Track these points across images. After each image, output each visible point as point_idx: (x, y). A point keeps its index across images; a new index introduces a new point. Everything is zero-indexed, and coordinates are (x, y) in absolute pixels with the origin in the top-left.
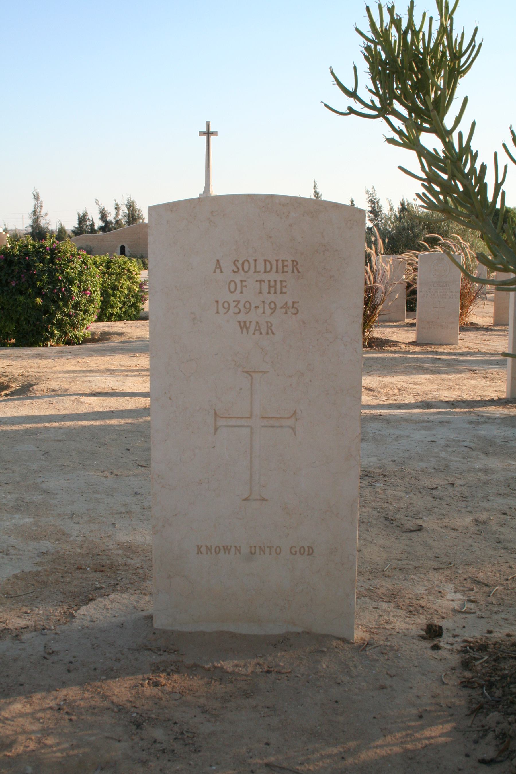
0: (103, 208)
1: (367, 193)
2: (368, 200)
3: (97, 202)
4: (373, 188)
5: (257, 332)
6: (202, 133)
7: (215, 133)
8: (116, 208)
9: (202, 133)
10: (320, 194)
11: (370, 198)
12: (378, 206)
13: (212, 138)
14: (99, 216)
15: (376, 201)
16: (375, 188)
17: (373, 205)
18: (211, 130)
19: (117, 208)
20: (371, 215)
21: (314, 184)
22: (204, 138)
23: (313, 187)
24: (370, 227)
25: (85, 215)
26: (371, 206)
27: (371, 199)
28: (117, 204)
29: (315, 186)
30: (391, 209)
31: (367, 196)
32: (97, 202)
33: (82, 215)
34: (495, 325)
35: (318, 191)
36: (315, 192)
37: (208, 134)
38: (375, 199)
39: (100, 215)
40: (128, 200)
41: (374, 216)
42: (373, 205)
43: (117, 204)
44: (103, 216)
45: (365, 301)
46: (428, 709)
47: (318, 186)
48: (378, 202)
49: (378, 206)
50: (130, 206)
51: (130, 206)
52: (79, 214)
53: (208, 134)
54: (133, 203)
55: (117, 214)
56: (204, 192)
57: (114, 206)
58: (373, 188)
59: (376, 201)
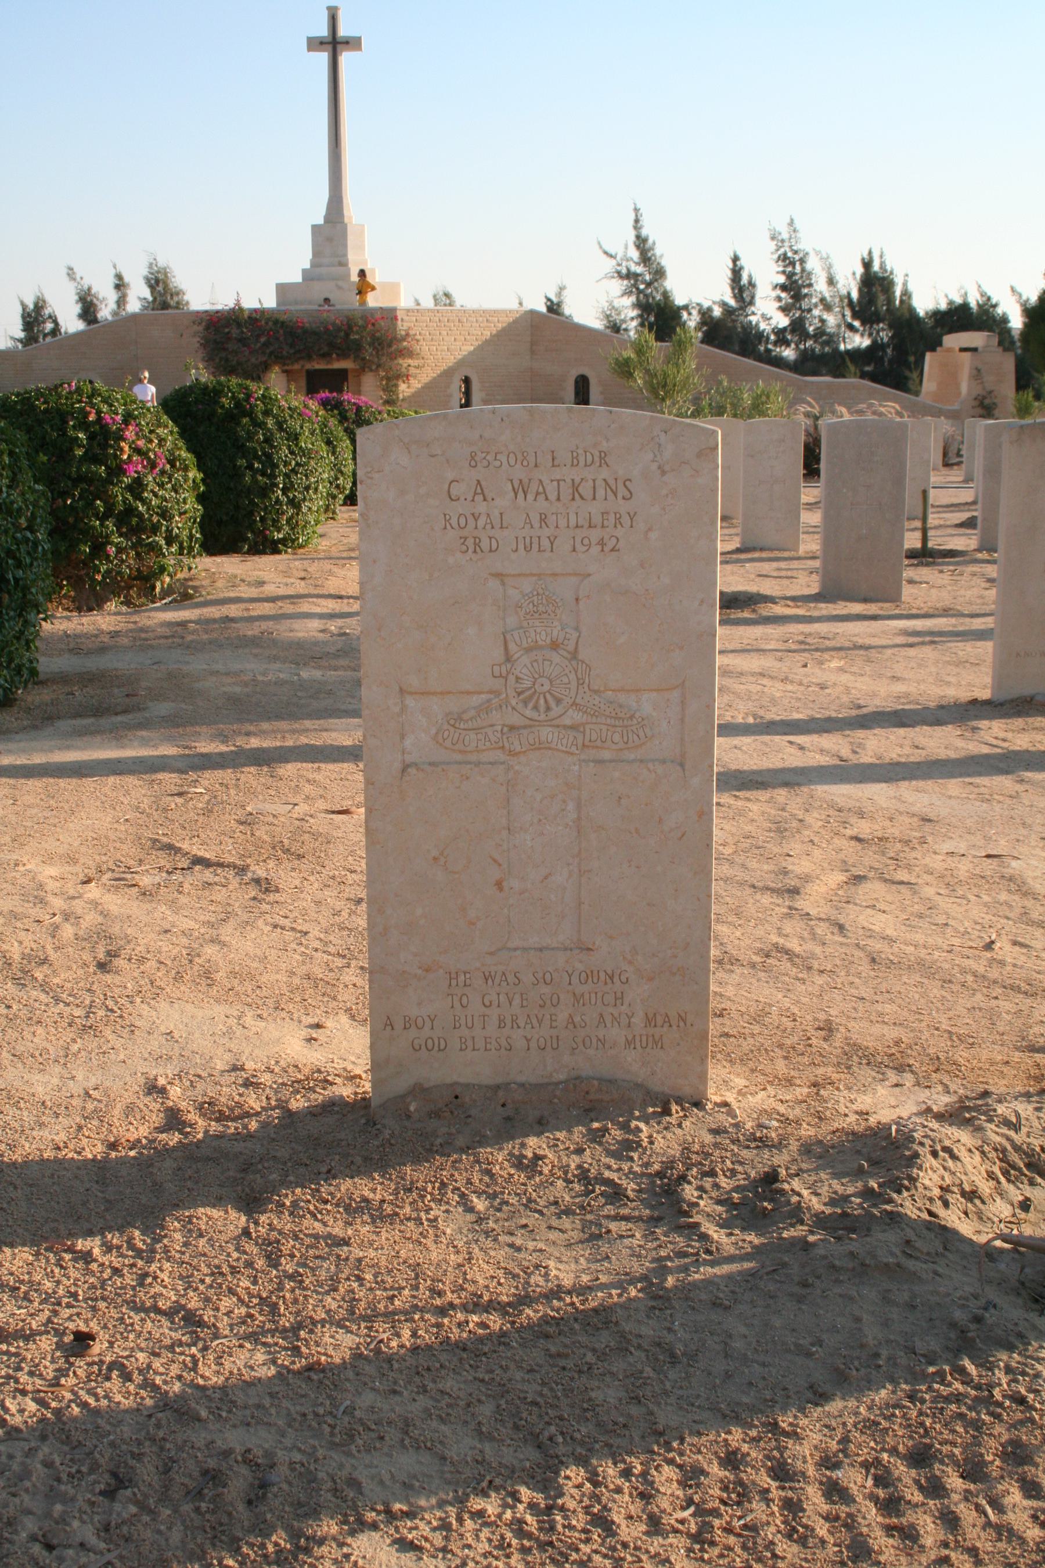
0: (86, 287)
1: (773, 238)
2: (776, 256)
3: (71, 274)
4: (791, 223)
5: (542, 497)
6: (315, 44)
7: (353, 43)
8: (118, 287)
9: (315, 44)
10: (650, 241)
11: (781, 251)
12: (803, 270)
13: (346, 58)
14: (77, 309)
15: (797, 257)
16: (797, 224)
17: (790, 269)
18: (343, 32)
19: (120, 285)
20: (783, 295)
21: (633, 217)
22: (323, 58)
23: (632, 223)
24: (780, 326)
25: (40, 306)
26: (784, 272)
27: (785, 254)
28: (119, 277)
29: (637, 221)
30: (831, 282)
31: (772, 245)
32: (71, 274)
33: (31, 306)
34: (979, 550)
35: (644, 232)
36: (638, 237)
37: (334, 45)
38: (796, 252)
39: (80, 305)
40: (151, 266)
41: (792, 297)
42: (790, 269)
43: (119, 277)
44: (88, 309)
45: (23, 317)
46: (837, 1263)
47: (645, 221)
48: (802, 261)
49: (803, 270)
50: (157, 281)
51: (157, 281)
52: (23, 304)
53: (334, 45)
54: (166, 274)
55: (121, 302)
56: (328, 219)
57: (111, 281)
58: (791, 223)
59: (797, 257)
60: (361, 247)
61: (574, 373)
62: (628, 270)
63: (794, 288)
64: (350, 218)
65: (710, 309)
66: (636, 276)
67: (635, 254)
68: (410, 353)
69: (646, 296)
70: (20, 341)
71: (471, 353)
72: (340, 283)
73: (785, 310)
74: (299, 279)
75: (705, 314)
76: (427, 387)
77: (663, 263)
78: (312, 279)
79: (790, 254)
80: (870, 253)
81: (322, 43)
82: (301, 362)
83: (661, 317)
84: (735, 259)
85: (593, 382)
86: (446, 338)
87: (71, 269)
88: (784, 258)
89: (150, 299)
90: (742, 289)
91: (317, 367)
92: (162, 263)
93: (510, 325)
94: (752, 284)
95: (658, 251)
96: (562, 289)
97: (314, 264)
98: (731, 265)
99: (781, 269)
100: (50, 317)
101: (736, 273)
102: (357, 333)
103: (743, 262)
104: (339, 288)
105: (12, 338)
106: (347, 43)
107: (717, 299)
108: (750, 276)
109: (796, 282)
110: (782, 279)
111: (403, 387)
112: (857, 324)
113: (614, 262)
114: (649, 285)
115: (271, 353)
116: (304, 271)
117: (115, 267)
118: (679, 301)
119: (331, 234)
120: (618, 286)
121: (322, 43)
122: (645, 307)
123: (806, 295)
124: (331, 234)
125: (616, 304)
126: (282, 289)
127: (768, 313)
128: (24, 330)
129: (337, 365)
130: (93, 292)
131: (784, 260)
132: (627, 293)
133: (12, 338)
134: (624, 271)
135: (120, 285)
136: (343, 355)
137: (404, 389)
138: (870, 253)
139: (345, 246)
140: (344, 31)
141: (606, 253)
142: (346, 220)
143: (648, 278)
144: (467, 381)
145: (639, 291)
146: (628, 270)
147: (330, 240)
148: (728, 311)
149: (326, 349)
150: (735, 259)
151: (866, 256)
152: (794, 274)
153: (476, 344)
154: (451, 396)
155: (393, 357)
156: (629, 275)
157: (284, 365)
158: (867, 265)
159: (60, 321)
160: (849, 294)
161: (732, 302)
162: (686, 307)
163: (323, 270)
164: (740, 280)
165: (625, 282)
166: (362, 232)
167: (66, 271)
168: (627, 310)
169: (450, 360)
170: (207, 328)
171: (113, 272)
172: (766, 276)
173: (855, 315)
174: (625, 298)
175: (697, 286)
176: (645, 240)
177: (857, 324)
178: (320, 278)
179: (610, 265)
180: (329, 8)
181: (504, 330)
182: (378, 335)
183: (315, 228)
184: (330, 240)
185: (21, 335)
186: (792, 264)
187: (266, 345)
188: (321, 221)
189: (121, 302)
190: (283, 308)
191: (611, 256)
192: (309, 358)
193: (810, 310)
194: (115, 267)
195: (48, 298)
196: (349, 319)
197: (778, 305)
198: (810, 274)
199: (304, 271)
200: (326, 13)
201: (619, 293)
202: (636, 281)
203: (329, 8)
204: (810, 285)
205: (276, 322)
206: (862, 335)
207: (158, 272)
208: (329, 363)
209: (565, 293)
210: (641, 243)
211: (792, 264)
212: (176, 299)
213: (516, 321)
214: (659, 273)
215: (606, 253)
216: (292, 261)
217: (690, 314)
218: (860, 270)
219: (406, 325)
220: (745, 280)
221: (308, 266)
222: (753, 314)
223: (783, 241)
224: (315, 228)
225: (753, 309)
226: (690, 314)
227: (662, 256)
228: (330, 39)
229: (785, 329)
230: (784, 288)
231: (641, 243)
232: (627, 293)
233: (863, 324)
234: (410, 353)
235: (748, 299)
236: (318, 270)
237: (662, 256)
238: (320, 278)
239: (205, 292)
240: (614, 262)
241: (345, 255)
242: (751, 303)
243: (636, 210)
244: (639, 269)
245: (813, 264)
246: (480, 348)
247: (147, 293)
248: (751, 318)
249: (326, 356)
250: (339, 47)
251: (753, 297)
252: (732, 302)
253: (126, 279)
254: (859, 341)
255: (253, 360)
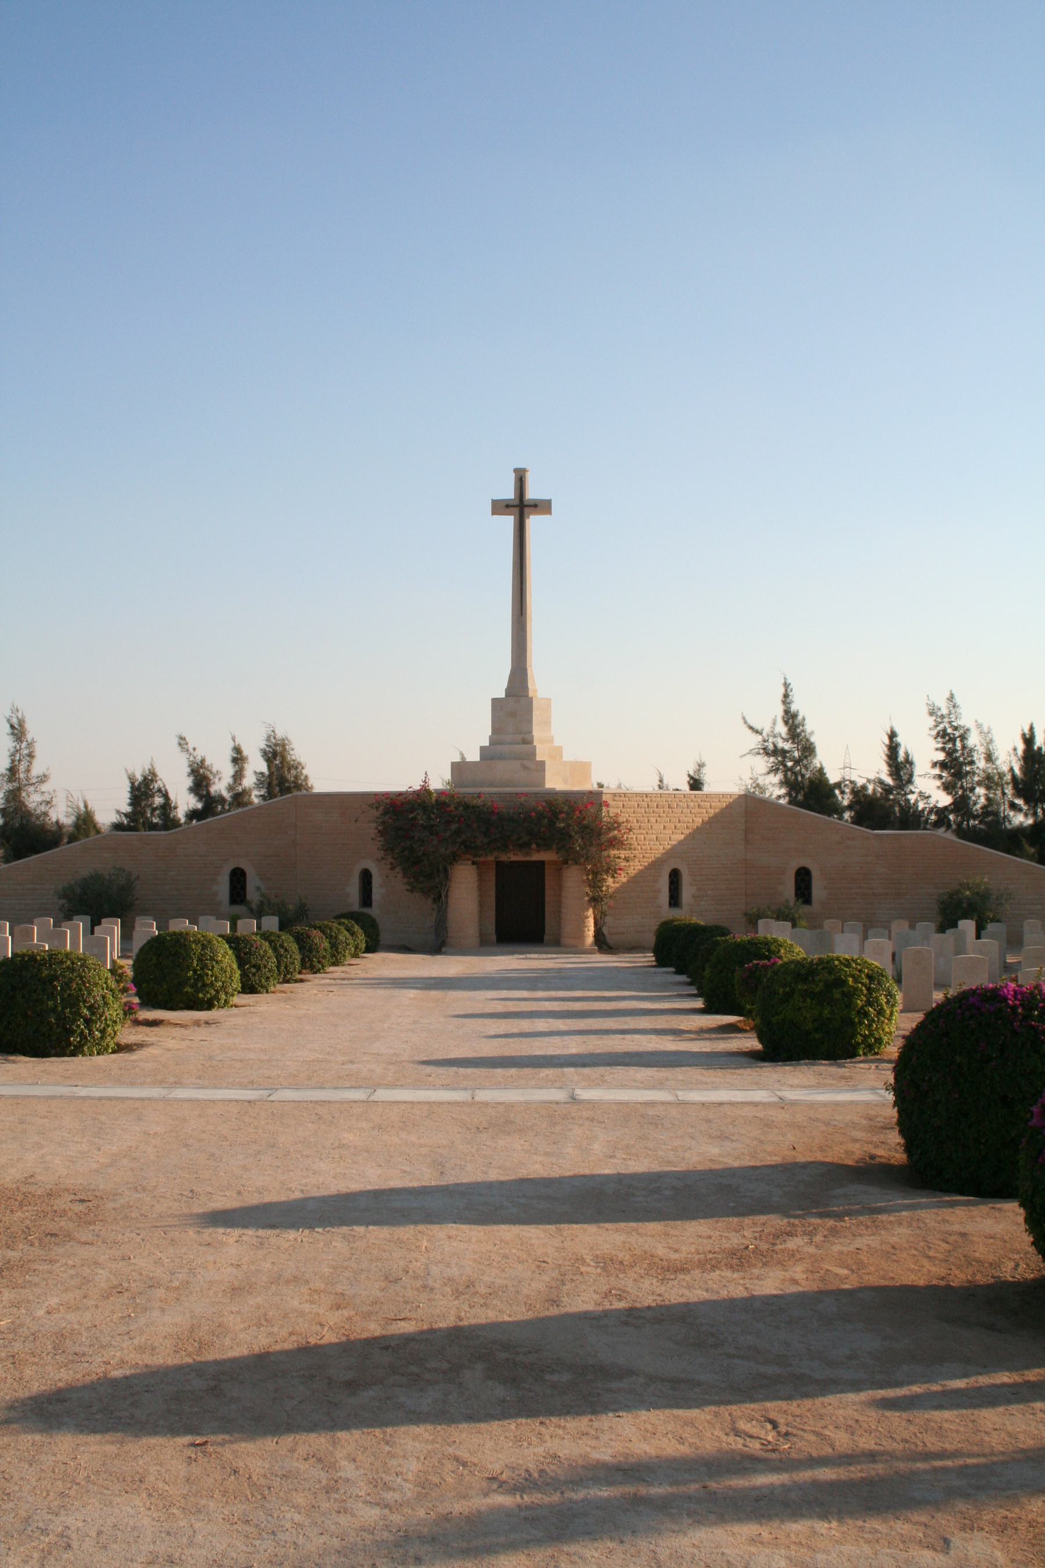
0: (199, 758)
1: (931, 714)
2: (934, 732)
3: (182, 742)
4: (951, 698)
6: (500, 507)
8: (235, 761)
9: (500, 507)
10: (800, 718)
12: (964, 747)
14: (189, 782)
15: (957, 734)
16: (958, 700)
17: (950, 746)
19: (238, 759)
21: (782, 691)
22: (508, 521)
23: (780, 697)
24: (940, 805)
26: (943, 749)
27: (945, 730)
28: (237, 750)
29: (786, 696)
30: (989, 758)
31: (931, 721)
32: (182, 742)
33: (140, 778)
35: (794, 708)
36: (787, 712)
37: (521, 507)
38: (956, 728)
40: (268, 739)
42: (950, 746)
43: (237, 750)
44: (200, 781)
48: (963, 738)
49: (964, 747)
50: (275, 754)
51: (275, 754)
53: (521, 507)
54: (284, 746)
55: (238, 776)
56: (509, 692)
57: (229, 753)
58: (951, 698)
59: (957, 734)
60: (547, 723)
61: (795, 864)
62: (775, 746)
63: (954, 766)
64: (535, 691)
65: (864, 788)
66: (784, 752)
67: (782, 729)
68: (616, 843)
69: (795, 774)
70: (126, 815)
71: (680, 843)
72: (525, 762)
73: (947, 788)
74: (477, 758)
75: (858, 793)
76: (633, 880)
77: (812, 739)
78: (492, 758)
79: (949, 731)
80: (1031, 729)
81: (507, 506)
82: (495, 854)
83: (812, 793)
84: (892, 735)
85: (815, 874)
86: (655, 826)
87: (182, 738)
88: (943, 734)
89: (267, 773)
90: (900, 767)
91: (514, 858)
92: (280, 734)
93: (723, 811)
94: (909, 762)
95: (809, 727)
96: (701, 766)
97: (493, 741)
98: (887, 742)
99: (940, 745)
100: (159, 790)
101: (893, 749)
102: (563, 820)
103: (899, 739)
104: (525, 768)
105: (118, 812)
106: (536, 506)
107: (872, 777)
108: (907, 754)
109: (956, 759)
110: (941, 756)
111: (610, 881)
112: (1019, 802)
113: (760, 738)
114: (797, 762)
115: (463, 842)
116: (482, 749)
117: (234, 740)
118: (833, 777)
119: (514, 709)
120: (762, 763)
121: (507, 506)
122: (792, 785)
123: (968, 773)
124: (514, 709)
125: (760, 781)
126: (459, 768)
127: (929, 790)
128: (130, 804)
129: (536, 857)
130: (207, 763)
131: (943, 737)
132: (774, 770)
133: (118, 812)
134: (771, 747)
135: (238, 759)
136: (545, 844)
137: (610, 883)
138: (1031, 729)
139: (530, 721)
140: (532, 493)
141: (751, 728)
142: (531, 694)
143: (796, 754)
144: (675, 877)
145: (787, 770)
146: (775, 746)
147: (513, 714)
148: (888, 790)
149: (526, 839)
150: (892, 735)
151: (1026, 731)
152: (956, 751)
153: (687, 832)
154: (659, 891)
155: (602, 847)
156: (776, 752)
157: (476, 856)
158: (1029, 740)
159: (172, 796)
160: (1011, 769)
161: (889, 781)
162: (838, 785)
163: (506, 748)
164: (897, 757)
165: (772, 759)
166: (549, 707)
167: (176, 740)
168: (774, 789)
169: (658, 850)
170: (386, 812)
171: (231, 744)
172: (924, 753)
173: (1019, 792)
174: (772, 775)
175: (850, 760)
176: (794, 716)
177: (1019, 802)
178: (501, 757)
179: (755, 741)
180: (516, 471)
181: (716, 816)
182: (585, 822)
183: (495, 702)
184: (513, 714)
185: (129, 809)
186: (953, 740)
187: (458, 832)
188: (502, 695)
189: (238, 776)
190: (457, 790)
191: (757, 732)
192: (505, 848)
193: (972, 789)
194: (234, 740)
195: (161, 773)
196: (550, 803)
197: (938, 783)
198: (971, 750)
199: (482, 749)
200: (512, 477)
201: (765, 770)
202: (784, 757)
203: (516, 471)
204: (972, 763)
205: (467, 806)
206: (1026, 815)
207: (276, 745)
208: (527, 854)
209: (704, 770)
210: (791, 718)
211: (953, 740)
212: (293, 772)
213: (729, 807)
214: (808, 750)
215: (751, 728)
216: (473, 737)
217: (842, 792)
218: (1021, 747)
219: (613, 811)
220: (901, 757)
221: (487, 743)
222: (912, 792)
223: (943, 717)
224: (495, 702)
225: (911, 787)
226: (842, 792)
227: (812, 733)
228: (517, 502)
229: (946, 808)
230: (943, 765)
231: (791, 718)
232: (774, 770)
233: (1027, 802)
234: (616, 843)
235: (905, 778)
236: (499, 748)
237: (812, 733)
238: (501, 757)
239: (337, 768)
240: (760, 738)
241: (531, 732)
242: (910, 781)
243: (786, 685)
244: (787, 746)
245: (974, 740)
246: (691, 837)
247: (263, 767)
248: (910, 797)
249: (524, 846)
250: (526, 510)
251: (911, 775)
252: (889, 781)
253: (245, 753)
254: (1020, 819)
255: (443, 850)
